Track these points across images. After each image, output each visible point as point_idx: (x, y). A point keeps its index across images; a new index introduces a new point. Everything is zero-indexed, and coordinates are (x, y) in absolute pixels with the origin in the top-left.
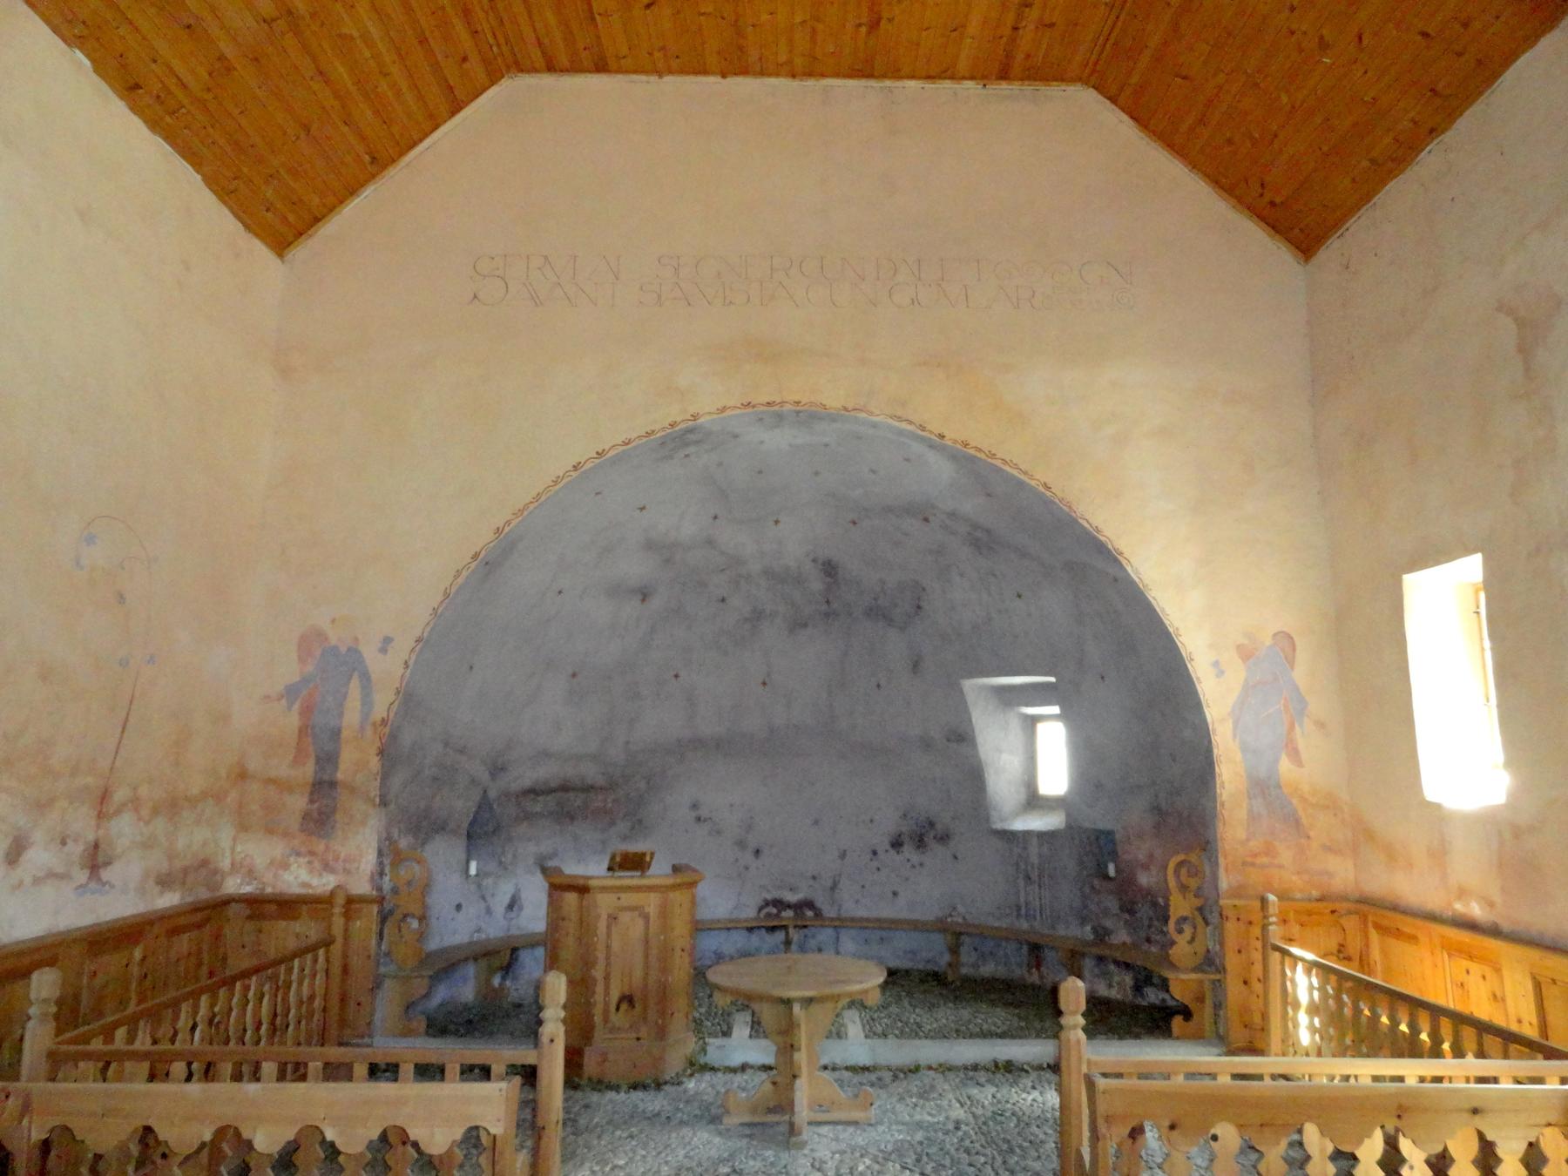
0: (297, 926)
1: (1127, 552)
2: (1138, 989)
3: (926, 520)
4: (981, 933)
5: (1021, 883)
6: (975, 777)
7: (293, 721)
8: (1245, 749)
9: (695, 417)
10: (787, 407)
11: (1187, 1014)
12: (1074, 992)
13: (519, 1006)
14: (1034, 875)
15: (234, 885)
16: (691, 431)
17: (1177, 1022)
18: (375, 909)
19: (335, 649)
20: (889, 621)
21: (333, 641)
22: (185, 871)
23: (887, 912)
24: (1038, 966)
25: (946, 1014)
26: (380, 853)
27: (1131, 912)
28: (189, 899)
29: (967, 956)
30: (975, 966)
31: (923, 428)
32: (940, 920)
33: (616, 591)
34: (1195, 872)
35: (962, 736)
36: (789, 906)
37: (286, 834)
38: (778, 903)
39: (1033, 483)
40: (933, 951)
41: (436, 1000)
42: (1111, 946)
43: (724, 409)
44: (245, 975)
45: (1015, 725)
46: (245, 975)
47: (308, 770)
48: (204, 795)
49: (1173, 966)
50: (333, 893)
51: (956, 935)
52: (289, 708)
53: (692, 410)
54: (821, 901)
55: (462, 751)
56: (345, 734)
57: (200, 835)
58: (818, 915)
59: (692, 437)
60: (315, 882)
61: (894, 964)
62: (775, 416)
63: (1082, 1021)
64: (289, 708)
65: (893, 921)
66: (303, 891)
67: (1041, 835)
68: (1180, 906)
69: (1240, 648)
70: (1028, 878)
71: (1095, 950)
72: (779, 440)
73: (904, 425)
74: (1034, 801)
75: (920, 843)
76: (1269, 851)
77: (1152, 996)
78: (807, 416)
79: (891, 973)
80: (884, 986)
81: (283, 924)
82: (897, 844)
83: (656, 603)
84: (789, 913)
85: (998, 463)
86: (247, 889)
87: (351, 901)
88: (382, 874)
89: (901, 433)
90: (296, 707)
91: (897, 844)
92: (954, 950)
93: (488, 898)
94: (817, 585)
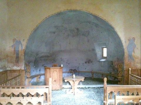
0: (15, 73)
1: (115, 27)
2: (115, 79)
3: (90, 23)
4: (96, 73)
5: (101, 67)
6: (96, 55)
7: (13, 49)
8: (128, 51)
9: (61, 11)
10: (73, 10)
11: (120, 82)
12: (105, 79)
13: (41, 82)
14: (103, 66)
15: (8, 69)
16: (60, 13)
17: (119, 83)
18: (25, 71)
19: (17, 41)
20: (85, 36)
21: (17, 40)
22: (3, 67)
23: (84, 71)
24: (103, 77)
25: (92, 82)
26: (25, 65)
27: (114, 70)
28: (4, 70)
29: (94, 75)
30: (95, 77)
31: (90, 12)
32: (91, 72)
33: (51, 32)
34: (122, 66)
35: (94, 50)
36: (73, 70)
37: (14, 63)
38: (71, 70)
39: (103, 19)
40: (90, 75)
41: (32, 81)
42: (112, 74)
43: (65, 10)
44: (11, 79)
45: (101, 48)
46: (11, 79)
47: (15, 55)
48: (4, 58)
49: (118, 77)
50: (20, 70)
51: (92, 73)
52: (12, 48)
53: (60, 10)
54: (77, 69)
55: (33, 53)
56: (19, 51)
57: (4, 63)
58: (76, 71)
59: (60, 13)
60: (17, 68)
61: (86, 77)
62: (71, 11)
63: (106, 82)
64: (12, 48)
65: (86, 72)
66: (15, 69)
67: (103, 61)
68: (120, 70)
69: (128, 39)
70: (102, 67)
71: (109, 75)
72: (72, 13)
73: (87, 12)
74: (103, 58)
75: (89, 63)
76: (130, 63)
77: (116, 80)
78: (75, 11)
79: (85, 78)
80: (84, 79)
81: (14, 73)
82: (86, 63)
83: (56, 34)
84: (73, 71)
85: (96, 15)
86: (9, 69)
87: (22, 70)
88: (25, 67)
89: (86, 13)
90: (13, 48)
91: (86, 63)
92: (93, 75)
93: (88, 89)
94: (76, 31)
